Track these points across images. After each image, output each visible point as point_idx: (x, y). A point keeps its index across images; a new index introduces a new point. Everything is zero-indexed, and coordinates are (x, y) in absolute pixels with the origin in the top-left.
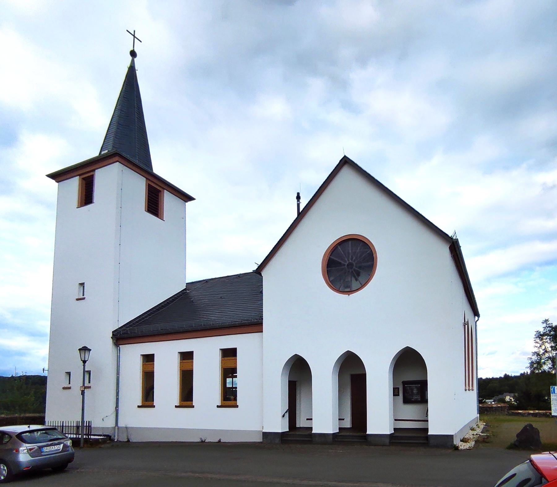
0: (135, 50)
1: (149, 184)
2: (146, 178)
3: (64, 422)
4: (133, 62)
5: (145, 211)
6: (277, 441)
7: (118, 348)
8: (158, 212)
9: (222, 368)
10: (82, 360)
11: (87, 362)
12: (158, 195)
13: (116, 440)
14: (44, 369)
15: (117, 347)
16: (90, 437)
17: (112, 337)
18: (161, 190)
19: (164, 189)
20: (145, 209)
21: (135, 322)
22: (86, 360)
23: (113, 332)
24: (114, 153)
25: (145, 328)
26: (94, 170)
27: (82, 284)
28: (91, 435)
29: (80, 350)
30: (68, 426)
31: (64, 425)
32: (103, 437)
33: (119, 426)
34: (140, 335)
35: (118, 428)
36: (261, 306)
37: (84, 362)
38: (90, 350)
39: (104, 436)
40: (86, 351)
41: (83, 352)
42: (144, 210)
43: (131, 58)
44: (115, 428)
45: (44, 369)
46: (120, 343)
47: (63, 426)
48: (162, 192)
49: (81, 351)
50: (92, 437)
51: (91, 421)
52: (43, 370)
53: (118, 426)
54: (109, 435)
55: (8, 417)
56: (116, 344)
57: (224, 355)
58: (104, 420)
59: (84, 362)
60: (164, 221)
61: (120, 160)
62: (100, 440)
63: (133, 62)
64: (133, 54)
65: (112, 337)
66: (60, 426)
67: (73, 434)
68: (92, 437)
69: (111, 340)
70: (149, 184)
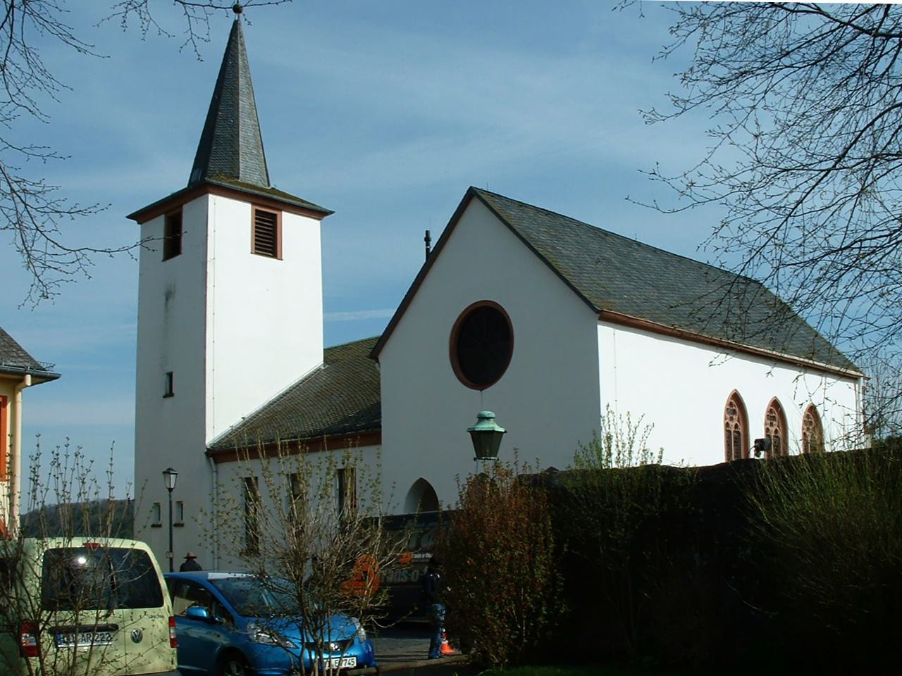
2: (253, 204)
19: (281, 210)
29: (164, 473)
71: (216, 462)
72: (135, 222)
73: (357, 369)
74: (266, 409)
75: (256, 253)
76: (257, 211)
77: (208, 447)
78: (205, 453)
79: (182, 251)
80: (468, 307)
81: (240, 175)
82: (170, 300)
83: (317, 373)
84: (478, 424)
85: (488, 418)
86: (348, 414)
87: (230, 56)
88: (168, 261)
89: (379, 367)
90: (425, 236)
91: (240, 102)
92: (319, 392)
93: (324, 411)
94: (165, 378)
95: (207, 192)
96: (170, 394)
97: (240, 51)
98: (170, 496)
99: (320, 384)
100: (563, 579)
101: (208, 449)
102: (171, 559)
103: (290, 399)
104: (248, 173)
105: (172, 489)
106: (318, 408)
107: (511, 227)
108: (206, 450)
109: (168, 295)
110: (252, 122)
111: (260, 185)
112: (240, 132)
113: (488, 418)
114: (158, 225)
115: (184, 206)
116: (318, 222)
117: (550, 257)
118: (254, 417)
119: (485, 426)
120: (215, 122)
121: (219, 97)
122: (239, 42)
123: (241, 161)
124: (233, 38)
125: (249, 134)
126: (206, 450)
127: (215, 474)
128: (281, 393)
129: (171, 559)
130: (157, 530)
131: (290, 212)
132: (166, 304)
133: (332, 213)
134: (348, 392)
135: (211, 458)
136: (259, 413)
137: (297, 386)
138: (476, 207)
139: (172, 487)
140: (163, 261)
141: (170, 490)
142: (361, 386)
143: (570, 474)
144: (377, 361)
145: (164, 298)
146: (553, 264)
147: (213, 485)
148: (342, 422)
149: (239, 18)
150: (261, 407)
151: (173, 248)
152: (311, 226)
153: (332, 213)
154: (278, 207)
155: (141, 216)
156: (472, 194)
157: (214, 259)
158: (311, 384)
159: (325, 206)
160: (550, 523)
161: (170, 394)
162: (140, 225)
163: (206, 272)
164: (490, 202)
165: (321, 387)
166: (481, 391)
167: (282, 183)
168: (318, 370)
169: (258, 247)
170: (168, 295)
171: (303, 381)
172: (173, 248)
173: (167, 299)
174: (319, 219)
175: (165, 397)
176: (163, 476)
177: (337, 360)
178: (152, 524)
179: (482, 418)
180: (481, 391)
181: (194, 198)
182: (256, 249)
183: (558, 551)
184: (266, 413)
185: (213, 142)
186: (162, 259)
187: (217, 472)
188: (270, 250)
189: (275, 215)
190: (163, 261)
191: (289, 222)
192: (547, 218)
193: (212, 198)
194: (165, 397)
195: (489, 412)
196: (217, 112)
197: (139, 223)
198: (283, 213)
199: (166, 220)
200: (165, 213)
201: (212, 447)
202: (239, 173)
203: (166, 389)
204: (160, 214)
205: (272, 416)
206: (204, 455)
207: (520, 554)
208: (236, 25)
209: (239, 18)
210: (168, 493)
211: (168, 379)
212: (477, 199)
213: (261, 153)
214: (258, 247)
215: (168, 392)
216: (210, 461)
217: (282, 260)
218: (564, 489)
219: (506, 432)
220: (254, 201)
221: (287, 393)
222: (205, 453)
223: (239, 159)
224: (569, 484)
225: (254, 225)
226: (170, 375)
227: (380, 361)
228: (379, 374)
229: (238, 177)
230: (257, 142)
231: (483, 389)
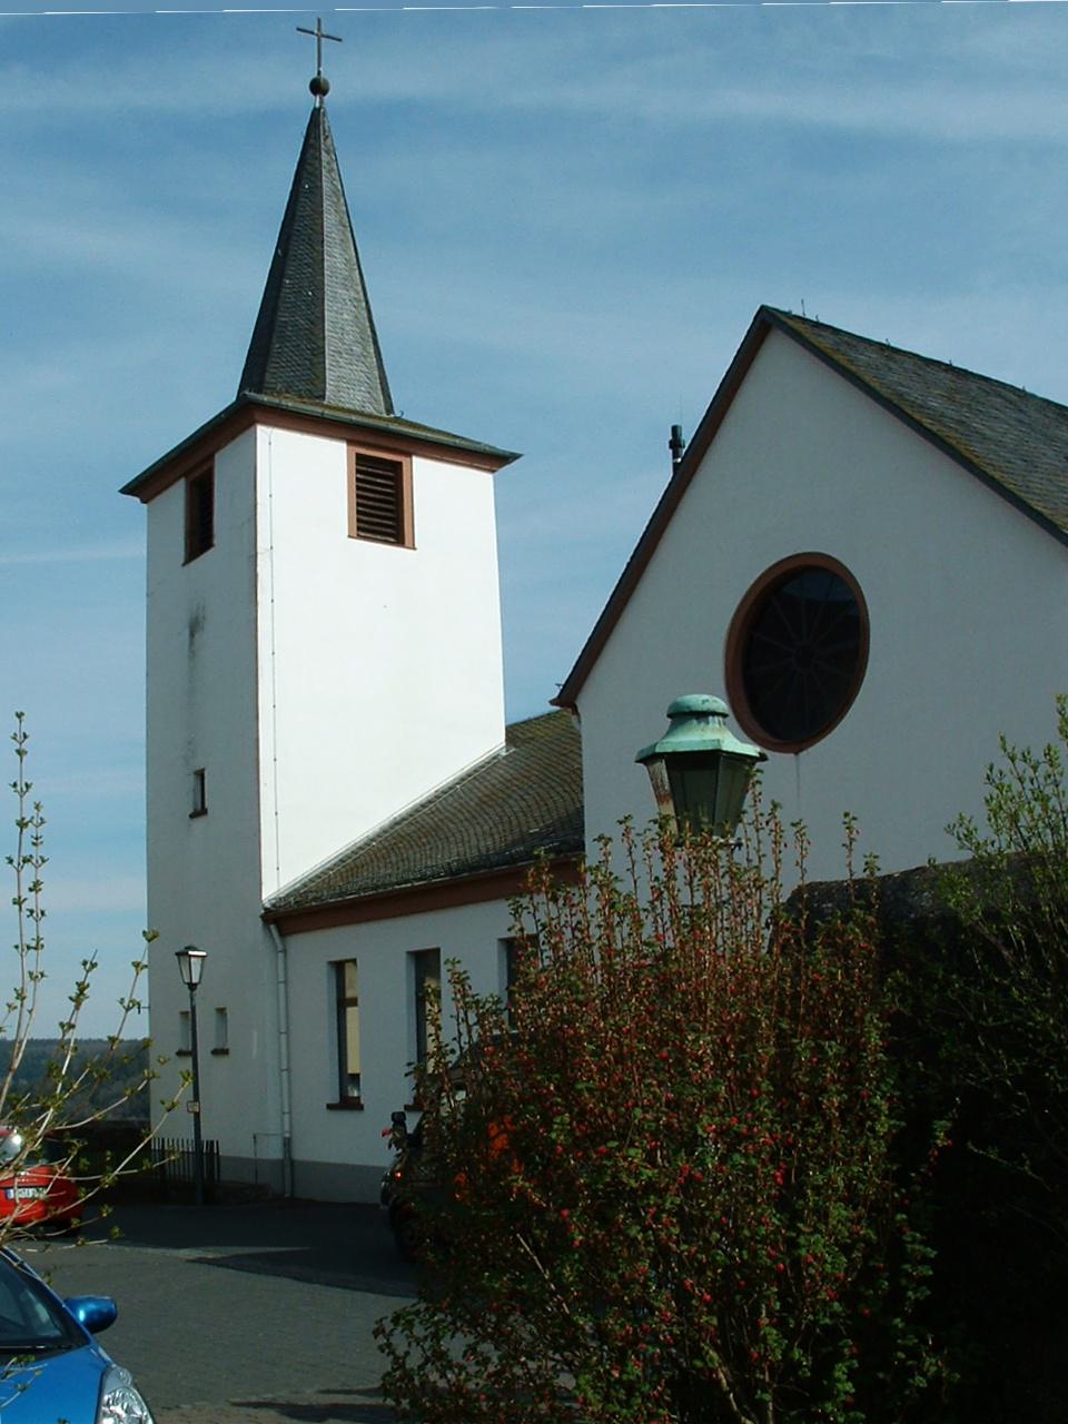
2: (350, 442)
19: (409, 455)
29: (177, 954)
49: (182, 958)
71: (283, 934)
72: (137, 500)
73: (565, 749)
74: (385, 832)
75: (359, 537)
76: (359, 457)
77: (268, 905)
78: (262, 917)
79: (215, 542)
80: (760, 578)
81: (327, 393)
82: (197, 636)
83: (492, 764)
84: (668, 733)
85: (702, 715)
86: (530, 828)
87: (305, 175)
88: (192, 564)
89: (580, 722)
90: (671, 438)
91: (326, 257)
92: (486, 796)
93: (486, 828)
94: (192, 781)
95: (252, 423)
96: (200, 812)
97: (324, 164)
98: (192, 999)
99: (494, 781)
100: (932, 1254)
101: (266, 909)
102: (197, 1115)
103: (433, 813)
104: (346, 387)
105: (196, 985)
106: (478, 823)
107: (859, 378)
108: (263, 911)
109: (195, 627)
110: (353, 294)
111: (369, 409)
112: (326, 313)
113: (702, 715)
114: (175, 498)
115: (217, 456)
116: (488, 477)
117: (953, 437)
118: (361, 848)
119: (693, 738)
120: (278, 297)
121: (285, 253)
122: (323, 146)
123: (327, 366)
124: (312, 141)
125: (346, 316)
126: (263, 911)
127: (281, 955)
128: (418, 801)
129: (197, 1115)
130: (223, 1060)
131: (432, 458)
132: (191, 643)
133: (515, 457)
134: (539, 790)
135: (272, 927)
136: (373, 840)
137: (450, 788)
138: (778, 350)
139: (195, 980)
140: (184, 565)
141: (192, 986)
142: (566, 777)
143: (981, 870)
144: (575, 711)
145: (187, 632)
146: (961, 448)
147: (278, 976)
148: (514, 844)
149: (321, 102)
150: (377, 829)
151: (199, 538)
152: (479, 482)
153: (515, 457)
154: (404, 447)
155: (145, 487)
156: (768, 323)
157: (272, 548)
158: (477, 783)
159: (503, 445)
160: (875, 1039)
161: (200, 812)
162: (145, 505)
163: (256, 575)
164: (813, 339)
165: (494, 785)
166: (796, 753)
167: (415, 406)
168: (494, 758)
169: (362, 525)
170: (195, 627)
171: (463, 779)
172: (199, 538)
173: (192, 635)
174: (493, 471)
175: (192, 816)
176: (176, 958)
177: (532, 739)
178: (212, 1048)
179: (682, 716)
180: (796, 753)
181: (233, 438)
182: (359, 529)
183: (906, 1147)
184: (386, 839)
185: (274, 336)
186: (182, 561)
187: (285, 951)
188: (389, 530)
189: (400, 463)
190: (184, 565)
191: (428, 479)
192: (949, 376)
193: (264, 433)
194: (192, 816)
195: (705, 697)
196: (281, 281)
197: (144, 502)
198: (414, 458)
199: (187, 485)
200: (185, 475)
201: (274, 905)
202: (324, 390)
203: (195, 803)
204: (180, 478)
205: (395, 844)
206: (260, 920)
207: (813, 1126)
208: (316, 117)
209: (321, 102)
210: (189, 992)
211: (199, 782)
212: (779, 332)
213: (372, 351)
214: (362, 525)
215: (199, 807)
216: (270, 931)
217: (414, 549)
218: (949, 921)
219: (763, 758)
220: (350, 437)
221: (430, 802)
222: (262, 917)
223: (324, 362)
224: (966, 903)
225: (354, 483)
226: (200, 775)
227: (580, 710)
228: (580, 736)
229: (323, 397)
230: (362, 332)
231: (801, 750)
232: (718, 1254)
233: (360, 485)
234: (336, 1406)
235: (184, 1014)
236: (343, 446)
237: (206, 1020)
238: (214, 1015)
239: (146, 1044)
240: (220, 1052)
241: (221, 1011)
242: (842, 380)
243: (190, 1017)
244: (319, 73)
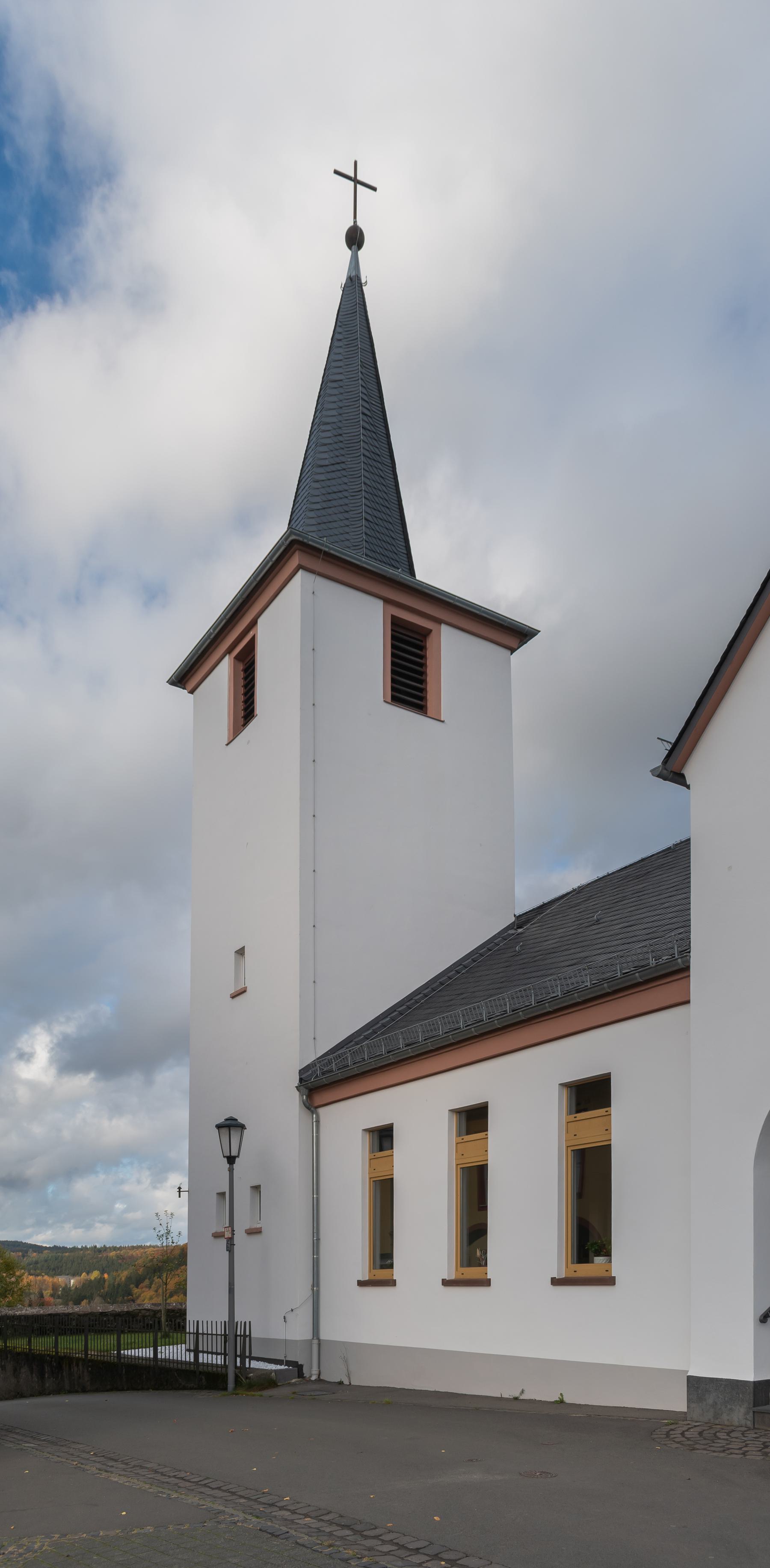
0: (360, 224)
1: (393, 616)
2: (387, 601)
3: (208, 1322)
4: (355, 263)
5: (385, 701)
6: (739, 1415)
7: (314, 1116)
8: (423, 698)
9: (570, 1149)
10: (224, 1157)
11: (237, 1159)
12: (423, 648)
13: (314, 1378)
14: (180, 1188)
15: (313, 1113)
16: (247, 1366)
17: (297, 1087)
18: (431, 628)
19: (439, 621)
20: (384, 696)
21: (362, 1037)
22: (232, 1155)
23: (300, 1071)
24: (288, 542)
25: (418, 1031)
26: (254, 623)
27: (241, 952)
28: (252, 1358)
29: (219, 1127)
30: (212, 1334)
31: (200, 1331)
32: (286, 1367)
33: (323, 1337)
34: (340, 1077)
35: (319, 1345)
36: (148, 1344)
37: (231, 1160)
38: (242, 1127)
39: (288, 1363)
40: (231, 1128)
41: (225, 1131)
42: (382, 699)
43: (349, 253)
44: (310, 1342)
45: (180, 1188)
46: (318, 1099)
47: (197, 1333)
48: (433, 634)
49: (221, 1129)
50: (255, 1364)
51: (250, 1322)
52: (180, 1192)
53: (319, 1340)
54: (297, 1362)
55: (111, 1308)
56: (308, 1105)
57: (578, 1104)
58: (287, 1319)
59: (231, 1160)
60: (443, 722)
61: (308, 562)
62: (273, 1374)
63: (355, 263)
64: (355, 239)
65: (297, 1087)
66: (194, 1333)
67: (217, 1354)
68: (255, 1364)
69: (297, 1093)
70: (393, 616)
96: (241, 952)
139: (234, 1153)
178: (248, 1227)
189: (429, 631)
232: (149, 1530)
233: (396, 652)
234: (248, 693)
235: (222, 1195)
236: (379, 604)
237: (242, 1195)
238: (248, 1191)
239: (187, 1244)
240: (254, 1232)
241: (257, 1188)
242: (569, 1037)
243: (227, 1197)
244: (355, 222)
